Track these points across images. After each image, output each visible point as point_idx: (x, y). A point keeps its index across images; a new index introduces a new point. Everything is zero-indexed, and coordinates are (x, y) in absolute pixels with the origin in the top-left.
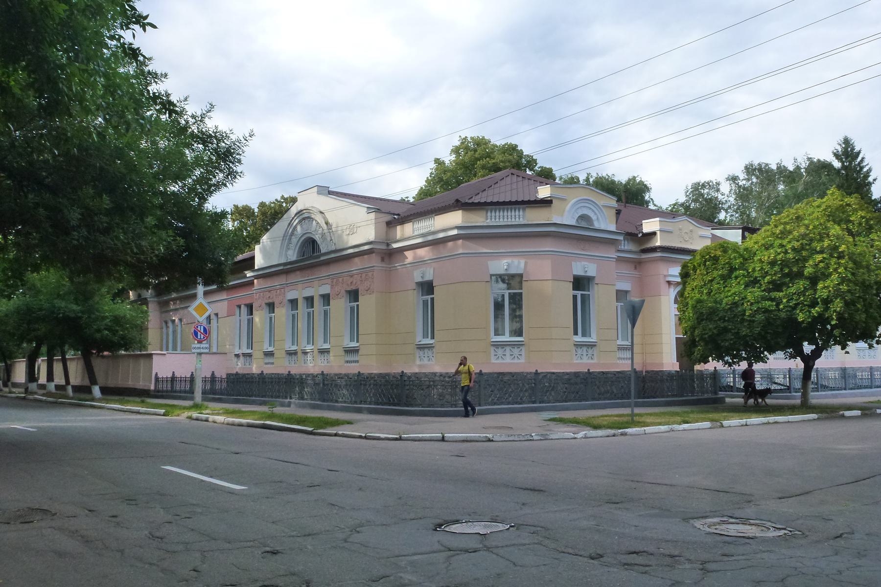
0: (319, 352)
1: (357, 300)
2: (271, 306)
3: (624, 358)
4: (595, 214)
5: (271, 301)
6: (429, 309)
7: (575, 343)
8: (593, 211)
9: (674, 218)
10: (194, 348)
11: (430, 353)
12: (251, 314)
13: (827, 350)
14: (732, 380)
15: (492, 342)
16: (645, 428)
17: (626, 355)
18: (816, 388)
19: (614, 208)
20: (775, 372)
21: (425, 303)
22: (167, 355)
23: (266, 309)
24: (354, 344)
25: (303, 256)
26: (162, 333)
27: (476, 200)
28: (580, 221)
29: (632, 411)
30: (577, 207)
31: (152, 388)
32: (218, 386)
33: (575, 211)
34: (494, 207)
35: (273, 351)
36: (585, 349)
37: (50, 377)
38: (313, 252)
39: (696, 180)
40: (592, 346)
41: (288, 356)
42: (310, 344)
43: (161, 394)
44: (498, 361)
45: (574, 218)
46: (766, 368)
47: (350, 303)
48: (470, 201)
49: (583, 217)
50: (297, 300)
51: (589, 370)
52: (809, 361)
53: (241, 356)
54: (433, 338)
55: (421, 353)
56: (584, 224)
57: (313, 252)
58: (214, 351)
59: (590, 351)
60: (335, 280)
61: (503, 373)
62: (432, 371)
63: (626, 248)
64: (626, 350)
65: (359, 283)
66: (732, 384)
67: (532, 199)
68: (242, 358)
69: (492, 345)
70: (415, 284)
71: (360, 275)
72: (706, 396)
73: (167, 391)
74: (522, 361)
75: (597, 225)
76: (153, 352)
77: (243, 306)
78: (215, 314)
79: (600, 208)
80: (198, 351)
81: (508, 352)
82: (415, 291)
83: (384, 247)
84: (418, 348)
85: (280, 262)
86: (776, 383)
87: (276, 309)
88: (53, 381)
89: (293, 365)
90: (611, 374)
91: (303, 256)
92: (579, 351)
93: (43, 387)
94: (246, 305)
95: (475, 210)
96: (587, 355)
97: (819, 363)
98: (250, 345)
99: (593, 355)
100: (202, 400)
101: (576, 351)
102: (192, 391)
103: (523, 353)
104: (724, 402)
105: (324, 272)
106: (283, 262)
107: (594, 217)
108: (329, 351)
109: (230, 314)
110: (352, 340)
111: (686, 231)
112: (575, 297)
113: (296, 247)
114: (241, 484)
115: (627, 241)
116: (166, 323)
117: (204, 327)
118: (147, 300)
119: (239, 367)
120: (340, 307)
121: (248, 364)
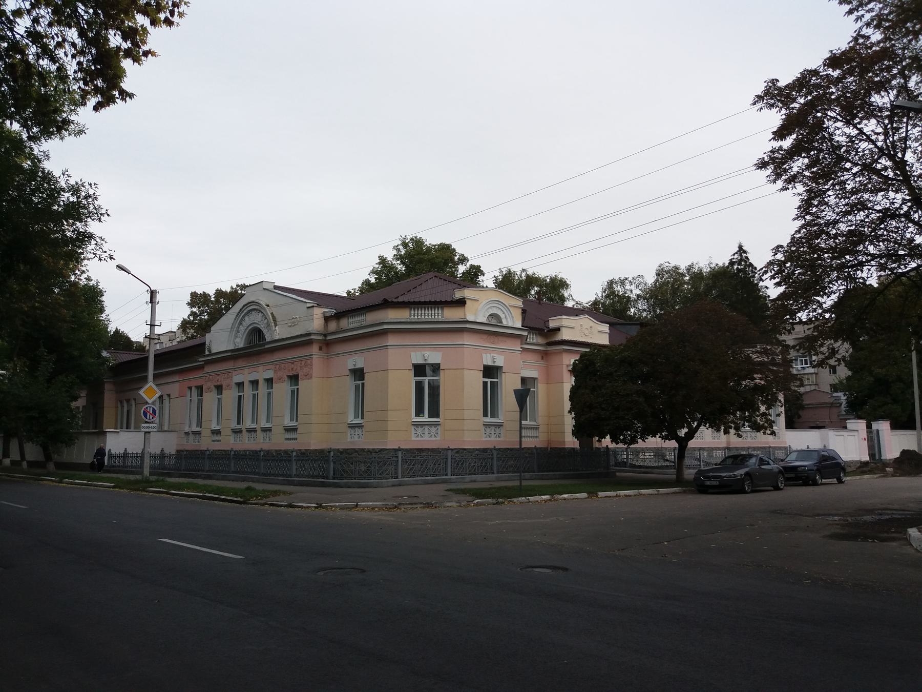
0: (262, 430)
2: (219, 388)
4: (504, 313)
5: (219, 384)
6: (360, 392)
8: (502, 310)
10: (144, 427)
11: (360, 431)
12: (201, 395)
16: (529, 498)
17: (534, 434)
21: (357, 387)
23: (215, 391)
27: (401, 299)
28: (490, 319)
29: (521, 483)
30: (486, 308)
32: (166, 462)
33: (486, 310)
34: (416, 306)
35: (220, 430)
36: (493, 428)
38: (259, 341)
40: (499, 426)
41: (234, 434)
44: (431, 439)
47: (354, 381)
48: (396, 301)
49: (493, 316)
50: (243, 383)
52: (683, 443)
53: (191, 434)
55: (353, 431)
56: (494, 322)
57: (259, 341)
58: (165, 429)
59: (498, 430)
60: (277, 367)
63: (534, 341)
64: (527, 429)
65: (299, 368)
66: (625, 460)
67: (449, 300)
70: (348, 371)
73: (119, 466)
75: (505, 323)
76: (107, 430)
77: (193, 388)
78: (167, 395)
79: (508, 308)
81: (426, 431)
84: (349, 427)
85: (228, 349)
87: (300, 382)
89: (253, 442)
92: (488, 430)
94: (197, 387)
95: (375, 310)
96: (495, 434)
97: (692, 444)
98: (199, 423)
101: (485, 430)
102: (141, 466)
106: (230, 349)
107: (502, 316)
108: (271, 430)
111: (587, 327)
112: (485, 384)
113: (244, 334)
115: (536, 335)
117: (153, 408)
119: (191, 444)
120: (282, 390)
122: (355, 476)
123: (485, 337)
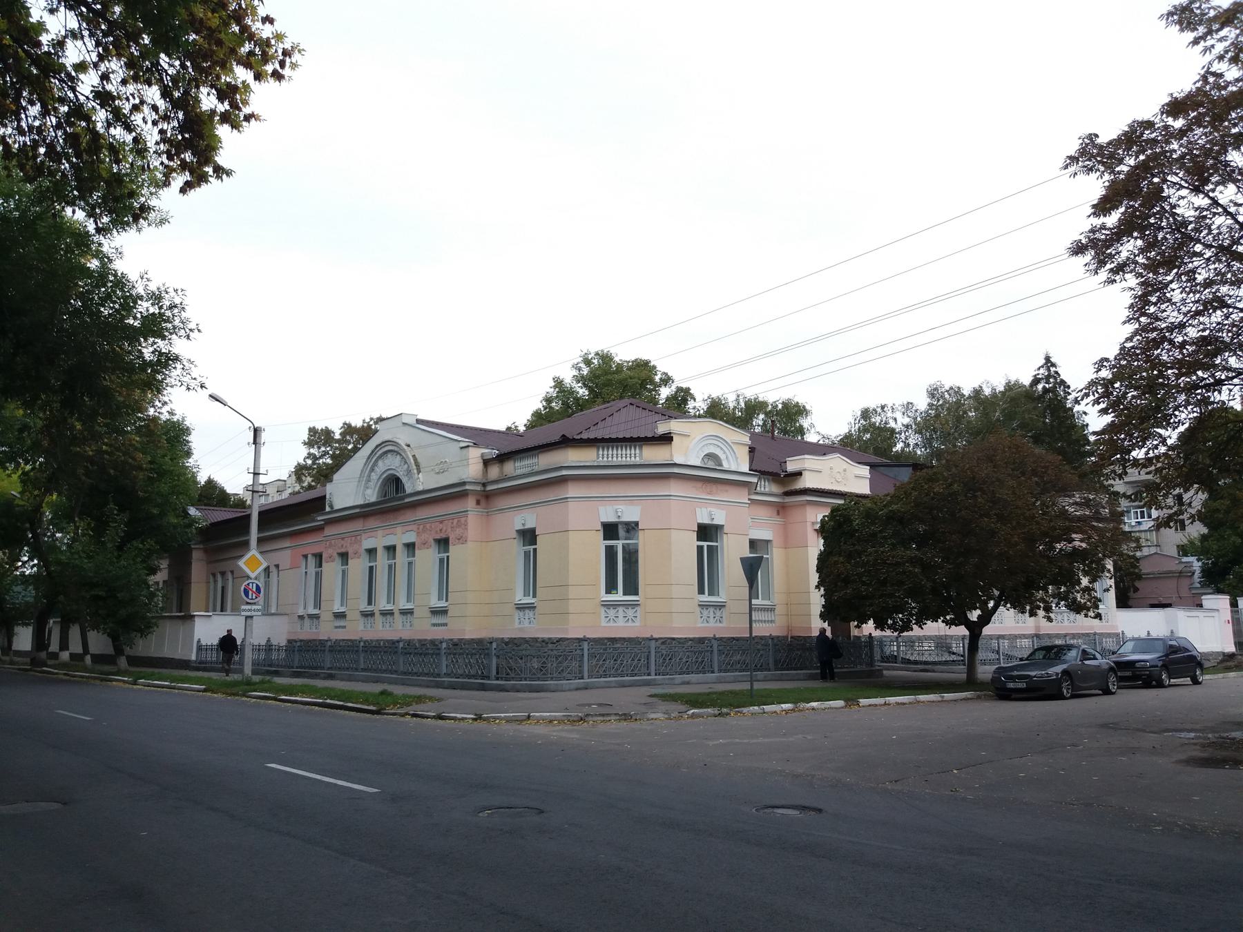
1: (447, 550)
2: (344, 557)
3: (765, 621)
4: (725, 453)
5: (343, 550)
6: (531, 561)
7: (700, 603)
8: (721, 449)
9: (824, 454)
11: (531, 614)
12: (320, 566)
13: (98, 632)
14: (895, 649)
15: (603, 601)
16: (764, 707)
18: (962, 660)
19: (748, 445)
20: (952, 639)
21: (527, 554)
22: (214, 617)
23: (338, 560)
24: (442, 604)
25: (385, 496)
26: (208, 589)
27: (585, 436)
28: (706, 460)
31: (193, 658)
32: (274, 656)
35: (344, 612)
36: (712, 610)
37: (64, 645)
38: (397, 493)
39: (866, 405)
40: (721, 606)
42: (390, 603)
43: (204, 665)
44: (609, 625)
45: (698, 457)
46: (941, 634)
48: (578, 437)
49: (710, 456)
51: (714, 635)
52: (975, 630)
54: (534, 596)
56: (711, 464)
57: (397, 493)
58: (273, 612)
59: (718, 613)
60: (422, 526)
61: (615, 638)
62: (532, 637)
64: (758, 610)
65: (449, 530)
66: (895, 654)
68: (307, 620)
69: (602, 605)
70: (515, 532)
71: (451, 521)
72: (859, 668)
74: (637, 624)
75: (726, 466)
76: (195, 613)
78: (275, 565)
80: (254, 607)
81: (621, 614)
82: (515, 541)
83: (479, 488)
84: (517, 608)
86: (954, 653)
87: (350, 561)
88: (67, 649)
90: (744, 640)
91: (385, 496)
92: (705, 612)
93: (55, 656)
96: (714, 617)
97: (987, 630)
99: (618, 617)
100: (252, 674)
101: (714, 612)
103: (638, 614)
104: (882, 675)
105: (410, 516)
107: (722, 457)
108: (393, 613)
109: (294, 567)
110: (440, 599)
112: (700, 549)
114: (89, 717)
116: (214, 575)
118: (190, 547)
119: (307, 632)
120: (427, 558)
121: (388, 625)
122: (525, 676)
123: (699, 484)
